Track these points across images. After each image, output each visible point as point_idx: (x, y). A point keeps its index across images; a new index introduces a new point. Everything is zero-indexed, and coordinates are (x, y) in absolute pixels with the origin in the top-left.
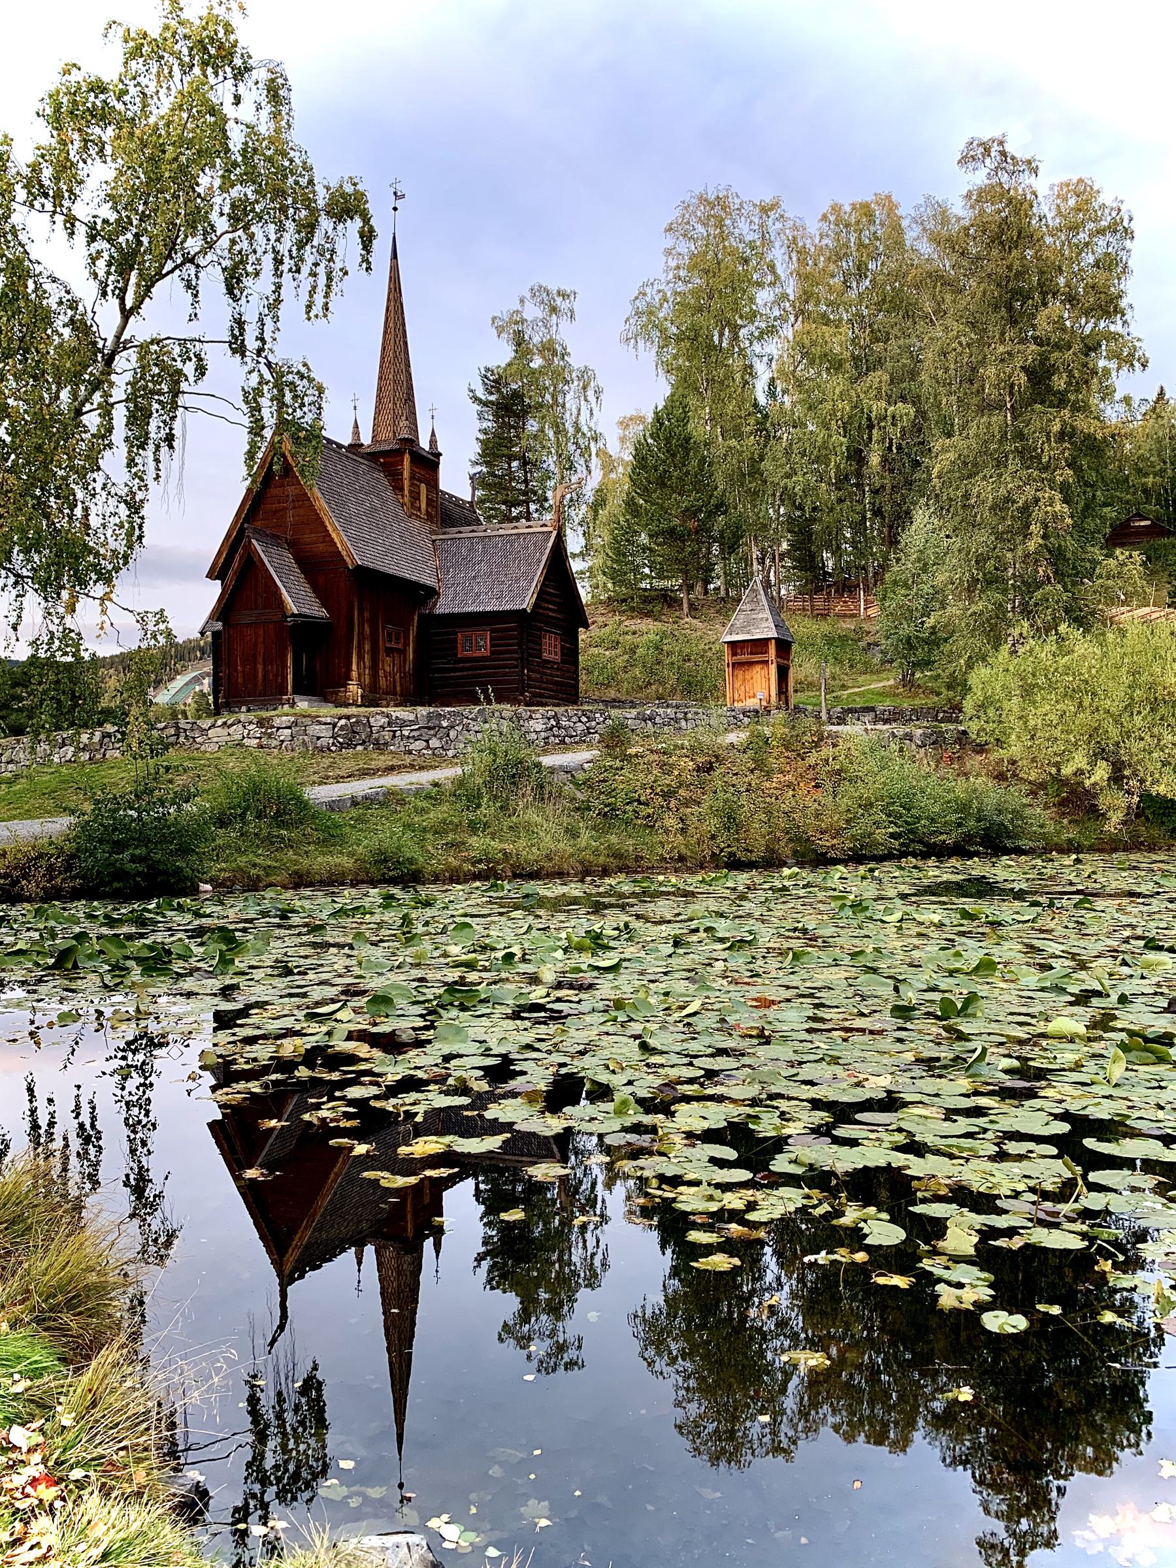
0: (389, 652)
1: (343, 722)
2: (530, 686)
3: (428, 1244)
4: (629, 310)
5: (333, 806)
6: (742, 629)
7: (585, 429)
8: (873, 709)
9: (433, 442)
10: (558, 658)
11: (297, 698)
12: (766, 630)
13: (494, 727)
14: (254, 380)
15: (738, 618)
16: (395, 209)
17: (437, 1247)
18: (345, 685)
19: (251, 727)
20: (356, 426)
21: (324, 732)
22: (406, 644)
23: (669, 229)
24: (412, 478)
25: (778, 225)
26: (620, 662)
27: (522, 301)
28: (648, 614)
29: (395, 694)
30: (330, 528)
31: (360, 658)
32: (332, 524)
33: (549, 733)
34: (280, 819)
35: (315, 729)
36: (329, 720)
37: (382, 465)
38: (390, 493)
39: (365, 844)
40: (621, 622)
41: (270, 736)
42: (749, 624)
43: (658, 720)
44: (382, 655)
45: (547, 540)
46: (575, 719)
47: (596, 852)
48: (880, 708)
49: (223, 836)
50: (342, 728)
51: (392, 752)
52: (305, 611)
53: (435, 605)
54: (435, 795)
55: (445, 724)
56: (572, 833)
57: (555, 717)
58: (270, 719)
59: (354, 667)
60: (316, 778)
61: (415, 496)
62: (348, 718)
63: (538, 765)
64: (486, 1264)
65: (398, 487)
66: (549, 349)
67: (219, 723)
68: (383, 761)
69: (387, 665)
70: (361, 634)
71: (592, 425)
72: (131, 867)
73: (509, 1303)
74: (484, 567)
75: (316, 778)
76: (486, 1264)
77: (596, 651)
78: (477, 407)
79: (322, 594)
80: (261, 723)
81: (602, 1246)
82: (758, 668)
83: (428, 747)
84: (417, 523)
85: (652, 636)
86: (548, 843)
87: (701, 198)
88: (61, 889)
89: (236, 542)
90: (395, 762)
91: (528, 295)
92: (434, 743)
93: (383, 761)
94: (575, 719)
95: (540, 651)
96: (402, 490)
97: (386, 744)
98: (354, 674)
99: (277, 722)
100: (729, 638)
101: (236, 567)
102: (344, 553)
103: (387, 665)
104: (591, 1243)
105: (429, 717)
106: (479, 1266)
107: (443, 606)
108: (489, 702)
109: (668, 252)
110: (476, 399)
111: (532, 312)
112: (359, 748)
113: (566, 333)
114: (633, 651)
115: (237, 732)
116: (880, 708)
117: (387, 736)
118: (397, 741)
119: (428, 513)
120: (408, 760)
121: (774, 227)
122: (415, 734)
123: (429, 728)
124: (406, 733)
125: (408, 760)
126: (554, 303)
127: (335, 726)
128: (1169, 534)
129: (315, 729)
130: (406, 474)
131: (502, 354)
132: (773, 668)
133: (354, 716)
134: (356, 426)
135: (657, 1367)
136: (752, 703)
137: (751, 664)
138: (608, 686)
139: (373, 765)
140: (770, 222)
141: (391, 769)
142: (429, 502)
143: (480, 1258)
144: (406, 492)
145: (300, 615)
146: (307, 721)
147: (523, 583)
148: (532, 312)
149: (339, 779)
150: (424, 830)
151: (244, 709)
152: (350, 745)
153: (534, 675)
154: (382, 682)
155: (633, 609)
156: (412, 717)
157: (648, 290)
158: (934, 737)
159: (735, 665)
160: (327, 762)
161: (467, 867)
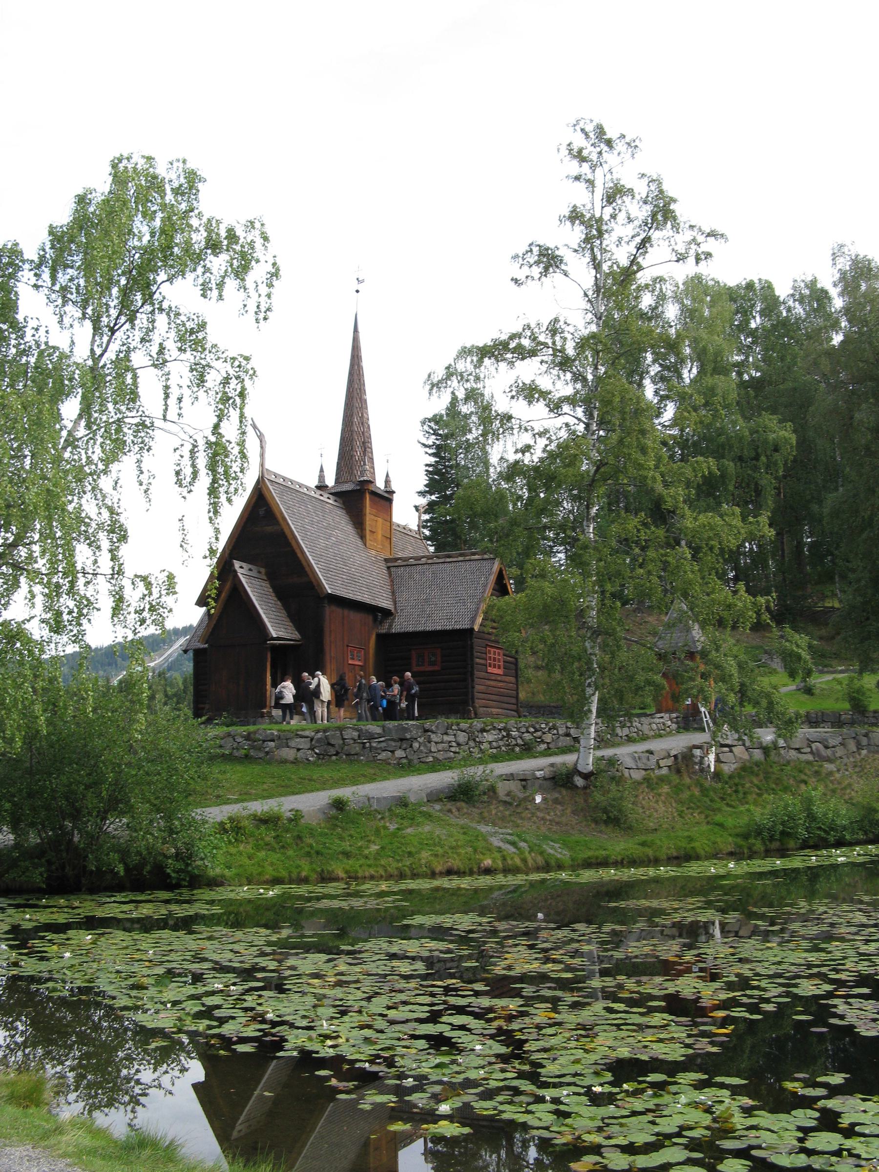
9: (387, 482)
13: (451, 738)
20: (322, 470)
33: (501, 743)
50: (319, 740)
92: (399, 753)
107: (400, 625)
117: (358, 748)
127: (312, 740)
134: (322, 470)
156: (379, 730)
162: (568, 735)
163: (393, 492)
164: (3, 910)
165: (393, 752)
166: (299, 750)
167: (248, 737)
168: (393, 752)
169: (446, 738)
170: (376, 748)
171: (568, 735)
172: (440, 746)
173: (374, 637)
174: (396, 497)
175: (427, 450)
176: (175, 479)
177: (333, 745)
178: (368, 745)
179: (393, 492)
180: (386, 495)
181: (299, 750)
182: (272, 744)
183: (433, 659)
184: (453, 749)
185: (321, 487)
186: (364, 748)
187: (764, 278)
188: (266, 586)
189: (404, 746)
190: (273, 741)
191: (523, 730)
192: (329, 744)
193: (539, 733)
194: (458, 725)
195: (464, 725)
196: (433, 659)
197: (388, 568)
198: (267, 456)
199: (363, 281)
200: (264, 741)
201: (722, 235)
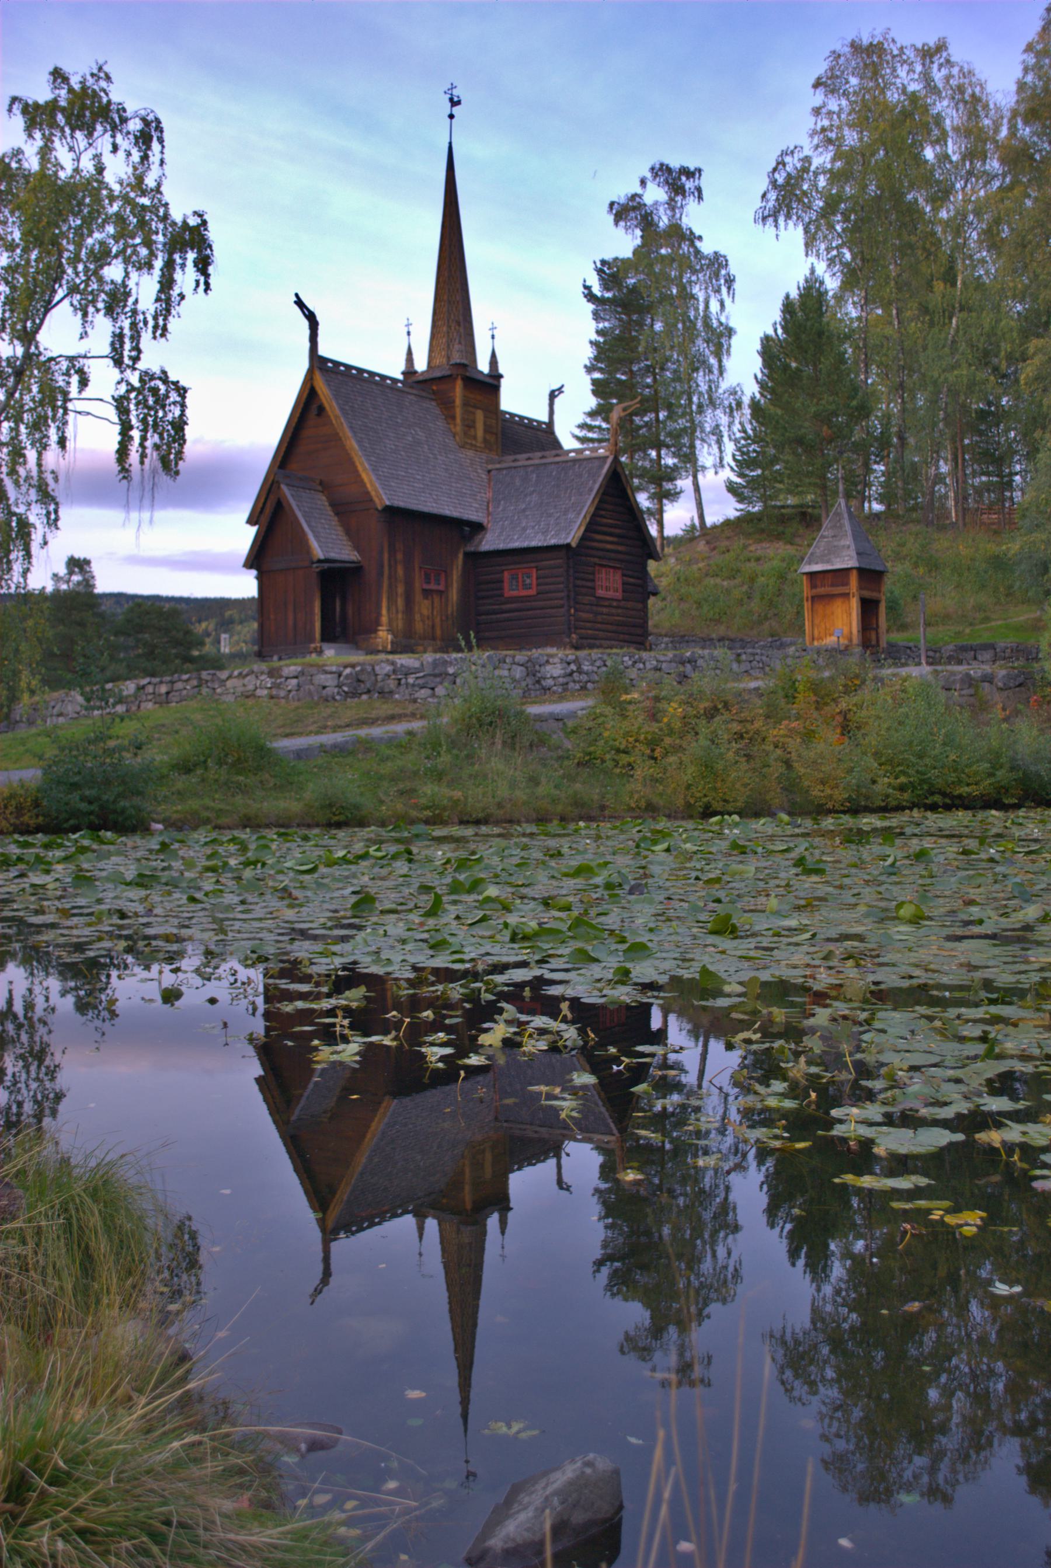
0: (427, 593)
1: (348, 671)
2: (576, 628)
3: (493, 1221)
4: (764, 184)
5: (300, 754)
6: (822, 560)
7: (715, 324)
8: (992, 646)
9: (494, 361)
10: (619, 595)
11: (325, 646)
12: (847, 560)
14: (123, 388)
15: (819, 546)
17: (503, 1224)
18: (376, 631)
19: (263, 677)
20: (410, 353)
21: (329, 681)
22: (448, 585)
23: (817, 85)
24: (466, 404)
25: (944, 71)
26: (737, 593)
27: (643, 182)
28: (779, 537)
29: (434, 638)
30: (360, 468)
31: (392, 600)
32: (362, 464)
34: (238, 766)
35: (321, 679)
36: (334, 669)
37: (434, 393)
38: (441, 423)
39: (312, 791)
40: (745, 547)
42: (833, 551)
43: (700, 662)
44: (418, 596)
45: (601, 467)
46: (598, 663)
47: (555, 801)
48: (1001, 644)
49: (181, 782)
50: (347, 677)
51: (397, 701)
52: (333, 555)
53: (481, 542)
54: (402, 745)
55: (451, 670)
56: (534, 781)
57: (576, 661)
58: (280, 669)
59: (384, 612)
60: (313, 728)
61: (469, 425)
62: (353, 666)
63: (522, 712)
64: (605, 1271)
65: (451, 418)
67: (236, 673)
68: (386, 709)
69: (424, 607)
70: (392, 577)
71: (723, 320)
72: (84, 806)
73: (635, 1314)
74: (535, 498)
75: (313, 728)
76: (605, 1271)
77: (712, 581)
78: (591, 307)
79: (353, 535)
80: (272, 673)
81: (735, 1256)
83: (433, 695)
84: (470, 453)
85: (776, 563)
86: (503, 791)
87: (853, 45)
88: (28, 825)
90: (398, 711)
91: (649, 175)
95: (594, 588)
96: (453, 418)
97: (391, 692)
98: (384, 619)
99: (286, 672)
100: (808, 569)
102: (373, 493)
103: (424, 607)
104: (721, 1251)
105: (435, 664)
106: (598, 1271)
107: (489, 542)
108: (470, 649)
109: (817, 111)
110: (590, 296)
111: (655, 194)
112: (365, 697)
113: (694, 217)
114: (752, 580)
115: (251, 682)
116: (1001, 644)
117: (392, 684)
118: (402, 688)
119: (485, 440)
120: (411, 708)
121: (938, 76)
122: (420, 681)
123: (435, 676)
125: (411, 708)
126: (678, 181)
127: (340, 676)
129: (321, 679)
130: (458, 402)
131: (624, 243)
132: (855, 603)
133: (358, 664)
135: (795, 1393)
136: (830, 641)
137: (831, 597)
138: (718, 621)
139: (374, 714)
140: (935, 66)
141: (391, 718)
142: (487, 430)
143: (599, 1264)
144: (458, 421)
145: (327, 561)
146: (313, 670)
147: (571, 516)
148: (655, 194)
149: (336, 728)
150: (381, 778)
151: (275, 658)
152: (354, 694)
153: (584, 615)
154: (419, 627)
155: (762, 531)
156: (417, 664)
157: (788, 159)
158: (1021, 679)
159: (814, 599)
160: (329, 711)
161: (414, 813)
162: (657, 669)
163: (501, 376)
164: (2, 863)
165: (433, 689)
168: (433, 689)
171: (915, 701)
173: (461, 556)
174: (503, 382)
175: (728, 302)
176: (172, 377)
178: (403, 681)
179: (501, 376)
180: (490, 381)
182: (294, 682)
183: (528, 581)
185: (409, 372)
188: (592, 510)
192: (359, 681)
194: (514, 657)
195: (521, 657)
196: (528, 581)
198: (320, 339)
199: (459, 103)
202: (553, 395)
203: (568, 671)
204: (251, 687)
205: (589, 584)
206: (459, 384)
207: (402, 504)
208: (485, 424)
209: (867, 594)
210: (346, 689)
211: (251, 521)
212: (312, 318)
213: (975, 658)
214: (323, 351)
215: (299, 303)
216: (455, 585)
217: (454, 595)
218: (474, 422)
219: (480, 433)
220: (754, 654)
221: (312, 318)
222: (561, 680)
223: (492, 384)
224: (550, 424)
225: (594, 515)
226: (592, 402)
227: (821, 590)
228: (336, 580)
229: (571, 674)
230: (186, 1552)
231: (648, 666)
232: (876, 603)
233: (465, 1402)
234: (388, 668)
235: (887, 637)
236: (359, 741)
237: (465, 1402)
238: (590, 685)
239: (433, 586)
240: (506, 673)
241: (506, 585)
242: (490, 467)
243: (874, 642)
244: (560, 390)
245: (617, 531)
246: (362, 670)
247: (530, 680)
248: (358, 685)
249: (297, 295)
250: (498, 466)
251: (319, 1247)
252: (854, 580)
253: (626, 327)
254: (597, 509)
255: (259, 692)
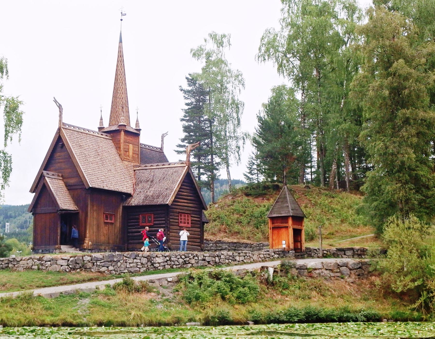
1: (72, 259)
8: (352, 249)
9: (137, 124)
11: (62, 247)
13: (139, 261)
16: (121, 20)
20: (101, 119)
21: (64, 263)
22: (115, 220)
27: (205, 41)
33: (166, 263)
41: (42, 265)
50: (72, 261)
59: (88, 232)
66: (220, 62)
79: (76, 200)
82: (283, 230)
89: (40, 178)
92: (111, 268)
93: (91, 275)
94: (179, 257)
96: (120, 148)
98: (88, 235)
99: (45, 259)
101: (40, 188)
103: (104, 230)
105: (109, 256)
107: (134, 202)
111: (211, 46)
113: (228, 54)
118: (95, 267)
122: (103, 264)
124: (98, 263)
127: (68, 261)
128: (4, 301)
131: (197, 67)
132: (291, 231)
134: (101, 119)
156: (101, 257)
158: (360, 265)
159: (274, 228)
162: (204, 260)
163: (140, 130)
165: (108, 267)
166: (62, 266)
167: (39, 260)
168: (108, 267)
169: (135, 260)
170: (99, 265)
172: (131, 265)
173: (121, 208)
177: (78, 264)
178: (95, 264)
179: (140, 130)
181: (62, 266)
182: (49, 263)
184: (138, 266)
186: (94, 265)
187: (182, 114)
189: (113, 264)
190: (50, 261)
191: (179, 257)
192: (76, 263)
193: (188, 259)
197: (135, 171)
200: (46, 261)
201: (182, 90)
202: (163, 137)
203: (165, 260)
204: (30, 265)
205: (176, 221)
206: (123, 133)
207: (97, 187)
208: (133, 150)
209: (297, 227)
210: (71, 266)
211: (32, 191)
212: (60, 107)
213: (345, 254)
214: (64, 121)
215: (56, 101)
216: (118, 220)
217: (118, 224)
218: (128, 149)
219: (131, 153)
220: (246, 253)
221: (60, 107)
222: (162, 264)
223: (136, 135)
224: (161, 149)
225: (179, 191)
226: (183, 135)
227: (276, 225)
228: (68, 218)
229: (166, 262)
230: (186, 141)
231: (200, 258)
232: (300, 231)
233: (121, 41)
234: (89, 258)
235: (306, 245)
236: (77, 291)
237: (121, 41)
238: (174, 266)
239: (109, 221)
240: (139, 261)
241: (141, 221)
242: (135, 169)
243: (299, 247)
244: (166, 134)
245: (189, 198)
246: (78, 259)
247: (149, 264)
248: (77, 266)
249: (54, 98)
250: (138, 169)
251: (164, 146)
252: (290, 221)
253: (198, 101)
254: (180, 188)
255: (33, 267)
